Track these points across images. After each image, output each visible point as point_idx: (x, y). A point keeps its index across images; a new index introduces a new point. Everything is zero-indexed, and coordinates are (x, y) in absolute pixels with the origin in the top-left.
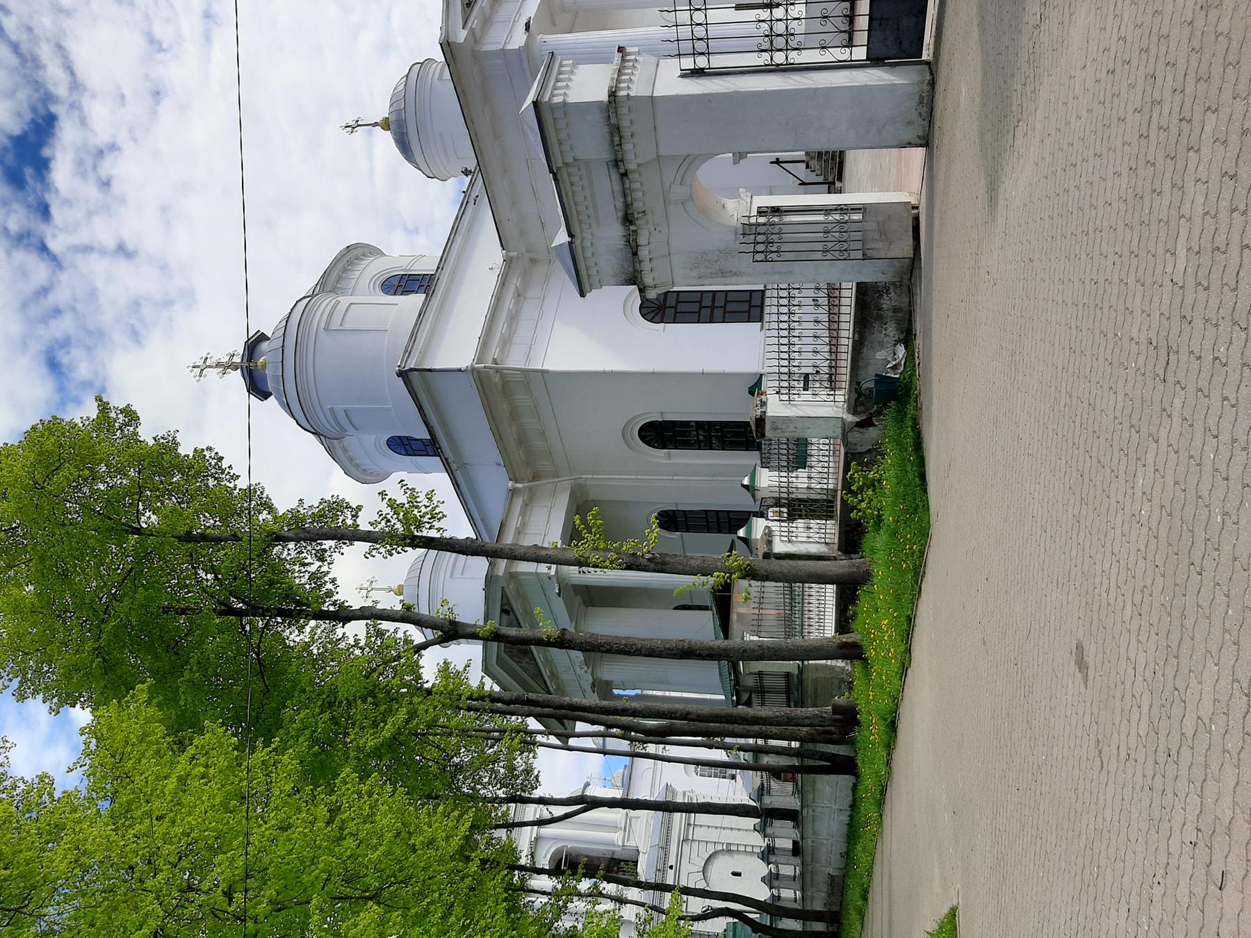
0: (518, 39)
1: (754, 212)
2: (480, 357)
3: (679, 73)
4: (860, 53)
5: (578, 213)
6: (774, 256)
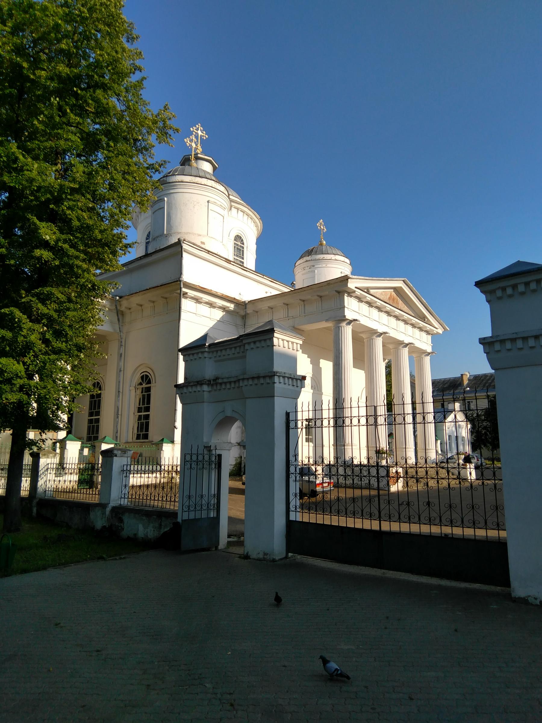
0: (349, 315)
1: (218, 452)
2: (189, 286)
3: (288, 411)
4: (296, 516)
5: (193, 354)
6: (189, 466)
